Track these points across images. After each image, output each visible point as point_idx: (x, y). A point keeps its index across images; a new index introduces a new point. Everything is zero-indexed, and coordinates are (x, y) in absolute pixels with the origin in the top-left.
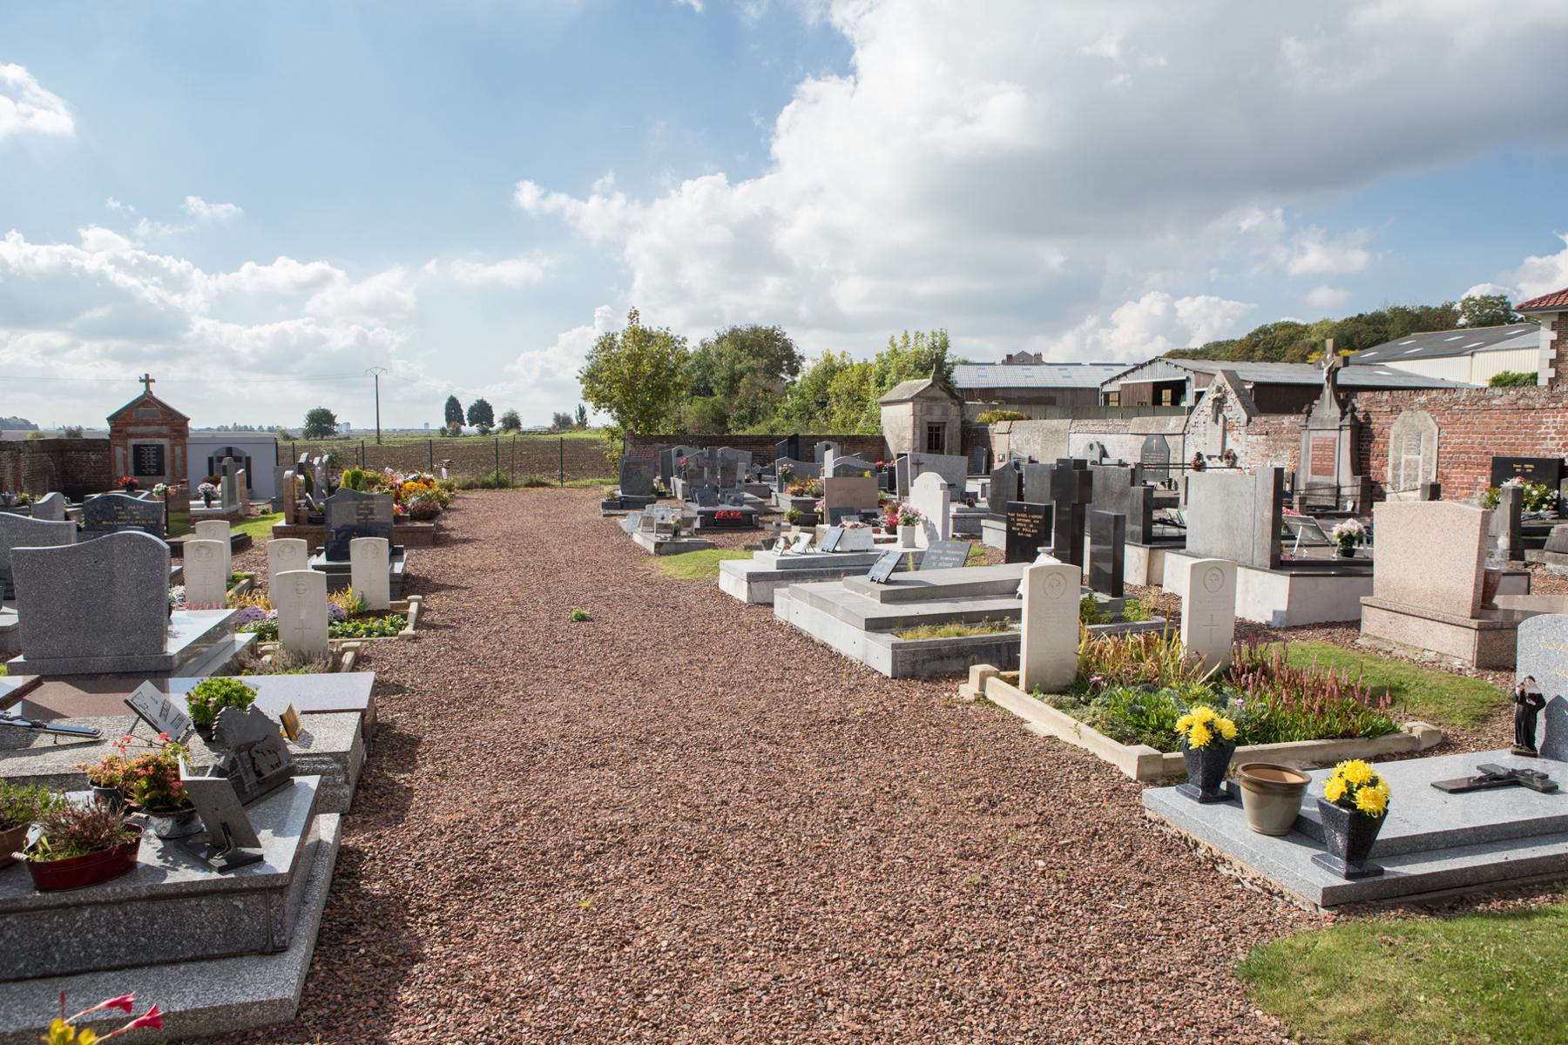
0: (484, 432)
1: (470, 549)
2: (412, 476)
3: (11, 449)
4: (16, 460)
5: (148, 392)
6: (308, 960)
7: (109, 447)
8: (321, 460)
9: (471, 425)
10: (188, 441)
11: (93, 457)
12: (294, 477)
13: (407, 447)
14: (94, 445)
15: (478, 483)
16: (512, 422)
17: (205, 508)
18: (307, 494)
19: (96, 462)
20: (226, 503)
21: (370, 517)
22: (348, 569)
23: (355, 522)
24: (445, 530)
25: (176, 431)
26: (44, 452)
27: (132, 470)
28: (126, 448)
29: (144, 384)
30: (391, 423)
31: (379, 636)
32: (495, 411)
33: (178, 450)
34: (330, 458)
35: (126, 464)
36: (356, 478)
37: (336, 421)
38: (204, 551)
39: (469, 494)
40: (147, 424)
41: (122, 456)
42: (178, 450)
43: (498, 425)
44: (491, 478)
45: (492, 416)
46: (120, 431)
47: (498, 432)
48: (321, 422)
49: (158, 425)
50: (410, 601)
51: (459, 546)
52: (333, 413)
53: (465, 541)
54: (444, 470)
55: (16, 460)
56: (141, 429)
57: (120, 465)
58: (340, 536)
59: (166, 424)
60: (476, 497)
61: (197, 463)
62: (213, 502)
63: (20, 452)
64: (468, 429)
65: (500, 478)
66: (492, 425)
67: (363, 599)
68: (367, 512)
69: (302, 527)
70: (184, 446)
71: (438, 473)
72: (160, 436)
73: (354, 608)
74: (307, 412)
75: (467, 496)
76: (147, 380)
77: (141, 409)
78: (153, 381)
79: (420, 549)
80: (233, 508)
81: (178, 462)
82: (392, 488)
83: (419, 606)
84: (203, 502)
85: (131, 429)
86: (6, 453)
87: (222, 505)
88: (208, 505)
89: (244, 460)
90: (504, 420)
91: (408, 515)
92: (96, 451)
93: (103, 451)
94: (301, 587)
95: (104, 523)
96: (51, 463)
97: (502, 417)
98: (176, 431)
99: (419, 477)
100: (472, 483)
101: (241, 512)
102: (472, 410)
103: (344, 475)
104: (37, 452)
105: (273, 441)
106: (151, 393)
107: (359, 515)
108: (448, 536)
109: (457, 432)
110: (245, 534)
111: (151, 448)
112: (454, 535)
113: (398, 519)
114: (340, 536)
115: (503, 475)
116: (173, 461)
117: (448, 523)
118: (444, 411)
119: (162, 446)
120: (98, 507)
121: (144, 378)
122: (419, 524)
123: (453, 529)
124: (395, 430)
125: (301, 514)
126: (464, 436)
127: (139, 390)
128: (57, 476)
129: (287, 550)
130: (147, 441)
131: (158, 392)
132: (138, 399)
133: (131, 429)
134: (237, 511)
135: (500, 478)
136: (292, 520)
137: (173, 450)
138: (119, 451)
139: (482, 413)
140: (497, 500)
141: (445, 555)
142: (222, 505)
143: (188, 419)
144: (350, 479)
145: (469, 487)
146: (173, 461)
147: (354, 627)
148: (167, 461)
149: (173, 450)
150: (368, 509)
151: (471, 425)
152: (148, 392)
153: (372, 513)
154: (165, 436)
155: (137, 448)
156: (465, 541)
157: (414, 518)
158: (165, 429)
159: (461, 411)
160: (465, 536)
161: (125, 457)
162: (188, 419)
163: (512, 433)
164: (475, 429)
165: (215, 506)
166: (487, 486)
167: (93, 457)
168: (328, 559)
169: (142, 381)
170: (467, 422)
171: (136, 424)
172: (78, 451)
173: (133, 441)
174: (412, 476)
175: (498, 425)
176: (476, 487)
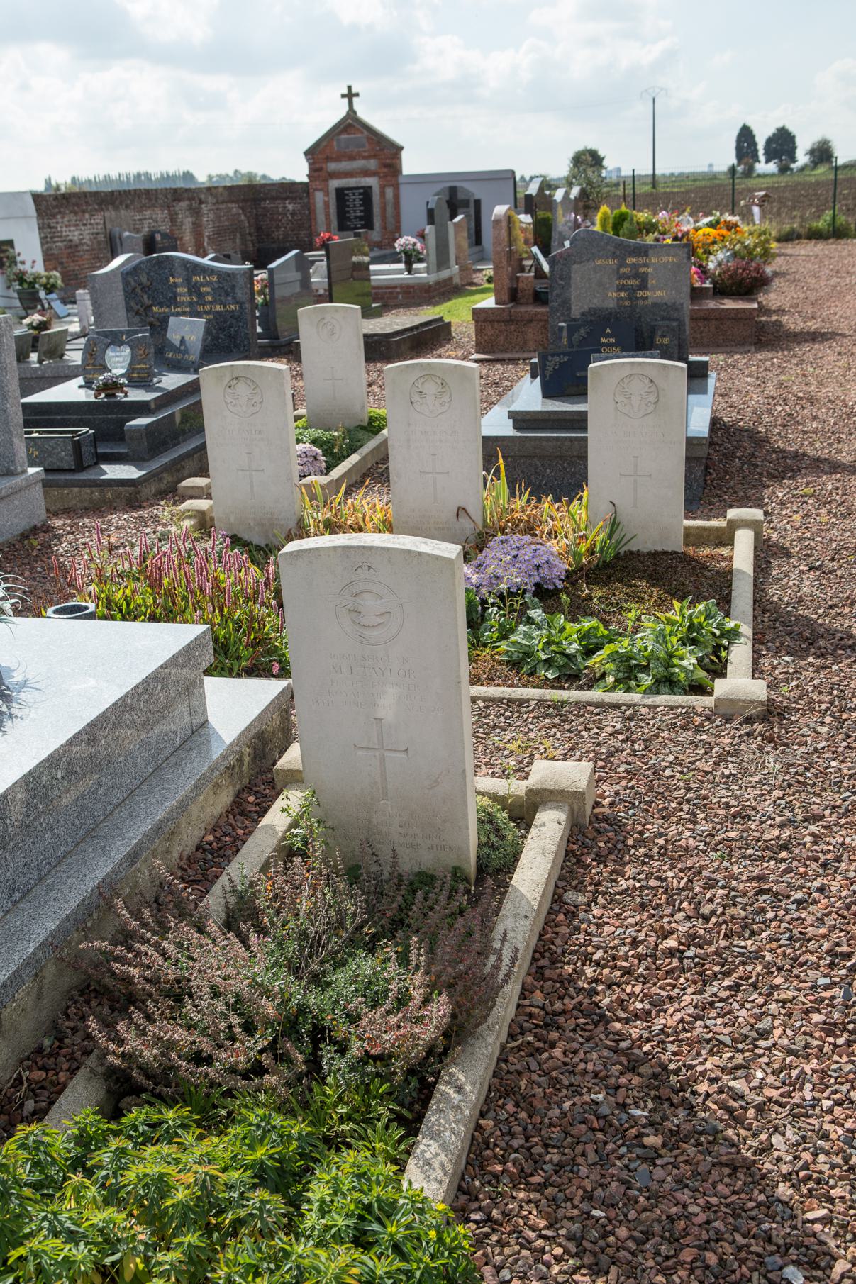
0: (784, 169)
1: (828, 353)
2: (706, 220)
3: (189, 199)
4: (196, 213)
5: (351, 112)
6: (537, 930)
7: (308, 193)
8: (567, 194)
9: (767, 161)
10: (401, 180)
11: (290, 207)
12: (509, 220)
13: (687, 192)
14: (287, 190)
15: (802, 231)
16: (822, 153)
17: (405, 275)
18: (535, 249)
19: (293, 214)
20: (434, 267)
21: (640, 294)
22: (579, 422)
23: (611, 305)
24: (768, 312)
25: (386, 166)
26: (232, 202)
27: (334, 224)
28: (327, 193)
29: (346, 100)
30: (665, 168)
31: (655, 690)
32: (798, 142)
33: (389, 192)
34: (583, 192)
35: (327, 216)
36: (619, 221)
37: (605, 163)
38: (242, 389)
39: (789, 249)
40: (351, 158)
41: (323, 202)
42: (389, 192)
43: (802, 158)
44: (822, 224)
45: (794, 148)
46: (320, 170)
47: (803, 169)
48: (588, 160)
49: (364, 158)
50: (734, 526)
51: (806, 347)
52: (601, 153)
53: (815, 337)
54: (756, 210)
55: (196, 213)
56: (345, 166)
57: (321, 217)
58: (576, 337)
59: (375, 156)
60: (803, 252)
61: (413, 208)
62: (415, 266)
63: (201, 202)
64: (765, 167)
65: (838, 223)
66: (794, 160)
67: (614, 525)
68: (636, 282)
69: (522, 309)
70: (396, 187)
71: (747, 216)
72: (366, 173)
73: (591, 551)
74: (571, 155)
75: (789, 251)
76: (350, 95)
77: (344, 136)
78: (357, 95)
79: (731, 353)
80: (445, 274)
81: (390, 210)
82: (675, 239)
83: (758, 536)
84: (402, 266)
85: (332, 166)
86: (184, 204)
87: (428, 270)
88: (410, 271)
89: (472, 204)
90: (812, 152)
91: (708, 285)
92: (293, 200)
93: (301, 199)
94: (370, 604)
95: (156, 309)
96: (243, 217)
97: (808, 146)
98: (386, 166)
99: (718, 222)
100: (793, 231)
101: (457, 280)
102: (769, 141)
103: (599, 215)
104: (223, 202)
105: (510, 175)
106: (355, 112)
107: (621, 288)
108: (779, 324)
109: (749, 172)
110: (441, 319)
111: (357, 192)
112: (793, 323)
113: (696, 294)
114: (576, 337)
115: (842, 219)
116: (384, 209)
117: (771, 298)
118: (734, 145)
119: (370, 188)
120: (144, 279)
121: (346, 92)
122: (729, 304)
123: (780, 311)
124: (672, 174)
125: (521, 285)
126: (759, 176)
127: (340, 111)
128: (250, 234)
129: (431, 388)
130: (352, 182)
131: (364, 113)
132: (340, 123)
133: (332, 166)
134: (451, 279)
135: (838, 223)
136: (505, 297)
137: (383, 194)
138: (319, 198)
139: (782, 144)
140: (842, 258)
141: (782, 370)
142: (428, 270)
143: (402, 148)
144: (611, 221)
145: (786, 238)
146: (384, 209)
147: (584, 636)
148: (376, 210)
149: (383, 194)
150: (636, 275)
151: (767, 161)
152: (351, 112)
153: (643, 286)
154: (373, 174)
155: (340, 192)
156: (815, 337)
157: (721, 290)
158: (372, 164)
159: (755, 144)
160: (813, 326)
161: (327, 205)
162: (402, 148)
163: (821, 169)
164: (772, 167)
165: (418, 271)
166: (815, 235)
167: (290, 207)
168: (548, 393)
169: (343, 96)
170: (762, 158)
171: (338, 159)
172: (274, 199)
173: (335, 184)
174: (706, 220)
175: (802, 158)
176: (799, 237)
